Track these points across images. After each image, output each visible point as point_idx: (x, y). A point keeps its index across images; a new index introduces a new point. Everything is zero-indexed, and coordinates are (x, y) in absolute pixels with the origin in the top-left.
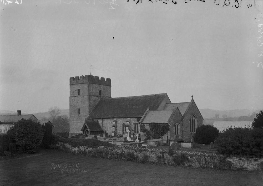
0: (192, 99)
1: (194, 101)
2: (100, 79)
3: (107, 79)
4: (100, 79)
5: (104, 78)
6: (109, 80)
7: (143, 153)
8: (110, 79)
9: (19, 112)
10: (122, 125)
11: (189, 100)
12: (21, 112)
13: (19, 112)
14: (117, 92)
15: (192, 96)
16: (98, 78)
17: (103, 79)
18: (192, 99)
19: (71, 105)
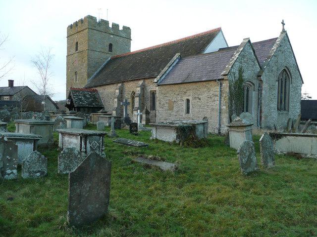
0: (283, 29)
1: (287, 34)
2: (110, 26)
3: (124, 27)
4: (110, 26)
5: (117, 26)
6: (127, 30)
7: (155, 212)
8: (129, 28)
9: (11, 82)
10: (130, 96)
11: (275, 33)
12: (14, 82)
13: (11, 82)
14: (137, 45)
15: (283, 24)
16: (106, 23)
17: (116, 26)
18: (283, 29)
19: (264, 45)
